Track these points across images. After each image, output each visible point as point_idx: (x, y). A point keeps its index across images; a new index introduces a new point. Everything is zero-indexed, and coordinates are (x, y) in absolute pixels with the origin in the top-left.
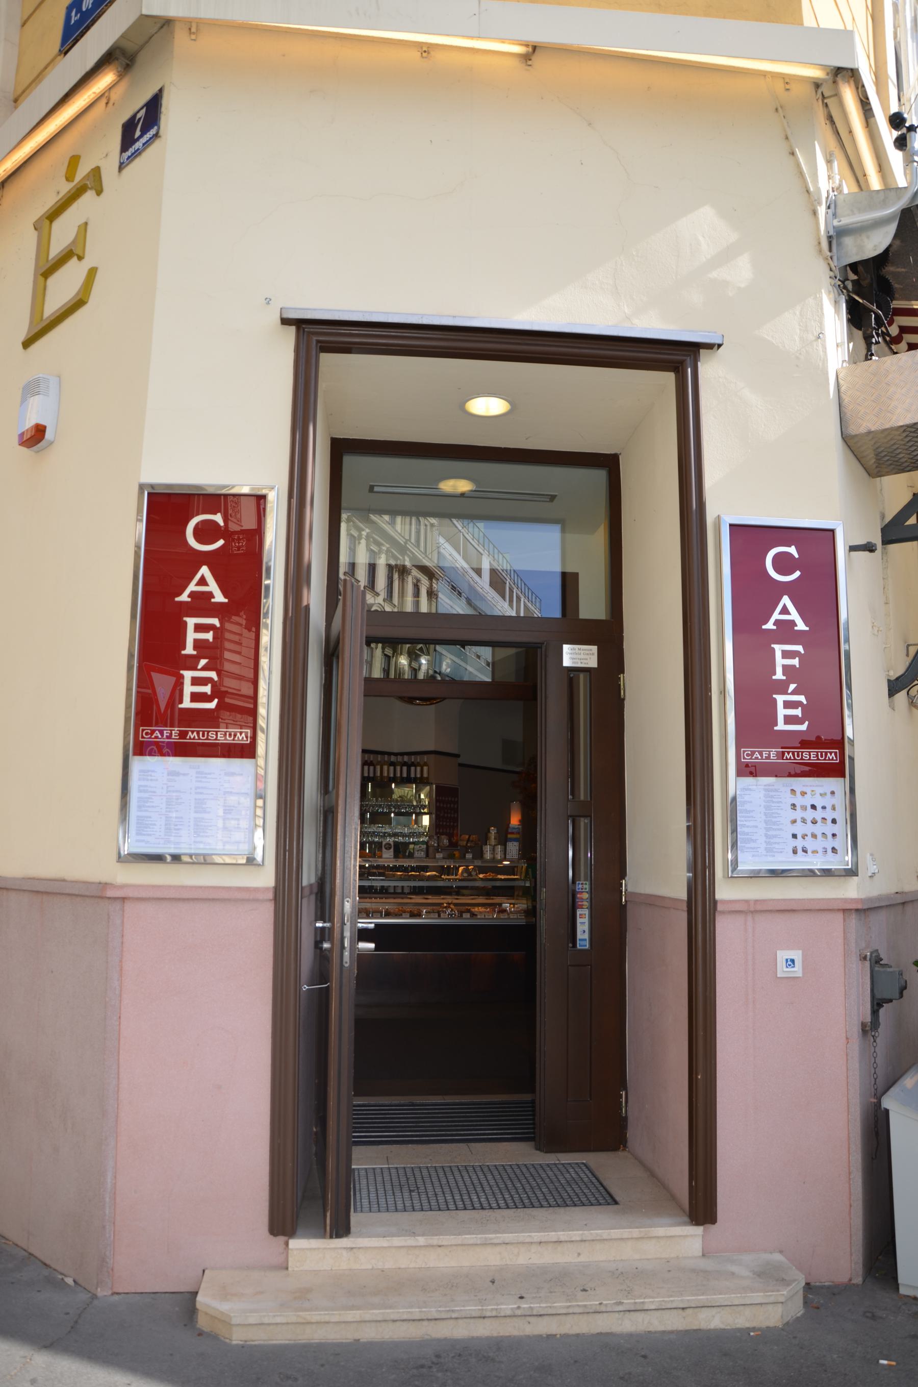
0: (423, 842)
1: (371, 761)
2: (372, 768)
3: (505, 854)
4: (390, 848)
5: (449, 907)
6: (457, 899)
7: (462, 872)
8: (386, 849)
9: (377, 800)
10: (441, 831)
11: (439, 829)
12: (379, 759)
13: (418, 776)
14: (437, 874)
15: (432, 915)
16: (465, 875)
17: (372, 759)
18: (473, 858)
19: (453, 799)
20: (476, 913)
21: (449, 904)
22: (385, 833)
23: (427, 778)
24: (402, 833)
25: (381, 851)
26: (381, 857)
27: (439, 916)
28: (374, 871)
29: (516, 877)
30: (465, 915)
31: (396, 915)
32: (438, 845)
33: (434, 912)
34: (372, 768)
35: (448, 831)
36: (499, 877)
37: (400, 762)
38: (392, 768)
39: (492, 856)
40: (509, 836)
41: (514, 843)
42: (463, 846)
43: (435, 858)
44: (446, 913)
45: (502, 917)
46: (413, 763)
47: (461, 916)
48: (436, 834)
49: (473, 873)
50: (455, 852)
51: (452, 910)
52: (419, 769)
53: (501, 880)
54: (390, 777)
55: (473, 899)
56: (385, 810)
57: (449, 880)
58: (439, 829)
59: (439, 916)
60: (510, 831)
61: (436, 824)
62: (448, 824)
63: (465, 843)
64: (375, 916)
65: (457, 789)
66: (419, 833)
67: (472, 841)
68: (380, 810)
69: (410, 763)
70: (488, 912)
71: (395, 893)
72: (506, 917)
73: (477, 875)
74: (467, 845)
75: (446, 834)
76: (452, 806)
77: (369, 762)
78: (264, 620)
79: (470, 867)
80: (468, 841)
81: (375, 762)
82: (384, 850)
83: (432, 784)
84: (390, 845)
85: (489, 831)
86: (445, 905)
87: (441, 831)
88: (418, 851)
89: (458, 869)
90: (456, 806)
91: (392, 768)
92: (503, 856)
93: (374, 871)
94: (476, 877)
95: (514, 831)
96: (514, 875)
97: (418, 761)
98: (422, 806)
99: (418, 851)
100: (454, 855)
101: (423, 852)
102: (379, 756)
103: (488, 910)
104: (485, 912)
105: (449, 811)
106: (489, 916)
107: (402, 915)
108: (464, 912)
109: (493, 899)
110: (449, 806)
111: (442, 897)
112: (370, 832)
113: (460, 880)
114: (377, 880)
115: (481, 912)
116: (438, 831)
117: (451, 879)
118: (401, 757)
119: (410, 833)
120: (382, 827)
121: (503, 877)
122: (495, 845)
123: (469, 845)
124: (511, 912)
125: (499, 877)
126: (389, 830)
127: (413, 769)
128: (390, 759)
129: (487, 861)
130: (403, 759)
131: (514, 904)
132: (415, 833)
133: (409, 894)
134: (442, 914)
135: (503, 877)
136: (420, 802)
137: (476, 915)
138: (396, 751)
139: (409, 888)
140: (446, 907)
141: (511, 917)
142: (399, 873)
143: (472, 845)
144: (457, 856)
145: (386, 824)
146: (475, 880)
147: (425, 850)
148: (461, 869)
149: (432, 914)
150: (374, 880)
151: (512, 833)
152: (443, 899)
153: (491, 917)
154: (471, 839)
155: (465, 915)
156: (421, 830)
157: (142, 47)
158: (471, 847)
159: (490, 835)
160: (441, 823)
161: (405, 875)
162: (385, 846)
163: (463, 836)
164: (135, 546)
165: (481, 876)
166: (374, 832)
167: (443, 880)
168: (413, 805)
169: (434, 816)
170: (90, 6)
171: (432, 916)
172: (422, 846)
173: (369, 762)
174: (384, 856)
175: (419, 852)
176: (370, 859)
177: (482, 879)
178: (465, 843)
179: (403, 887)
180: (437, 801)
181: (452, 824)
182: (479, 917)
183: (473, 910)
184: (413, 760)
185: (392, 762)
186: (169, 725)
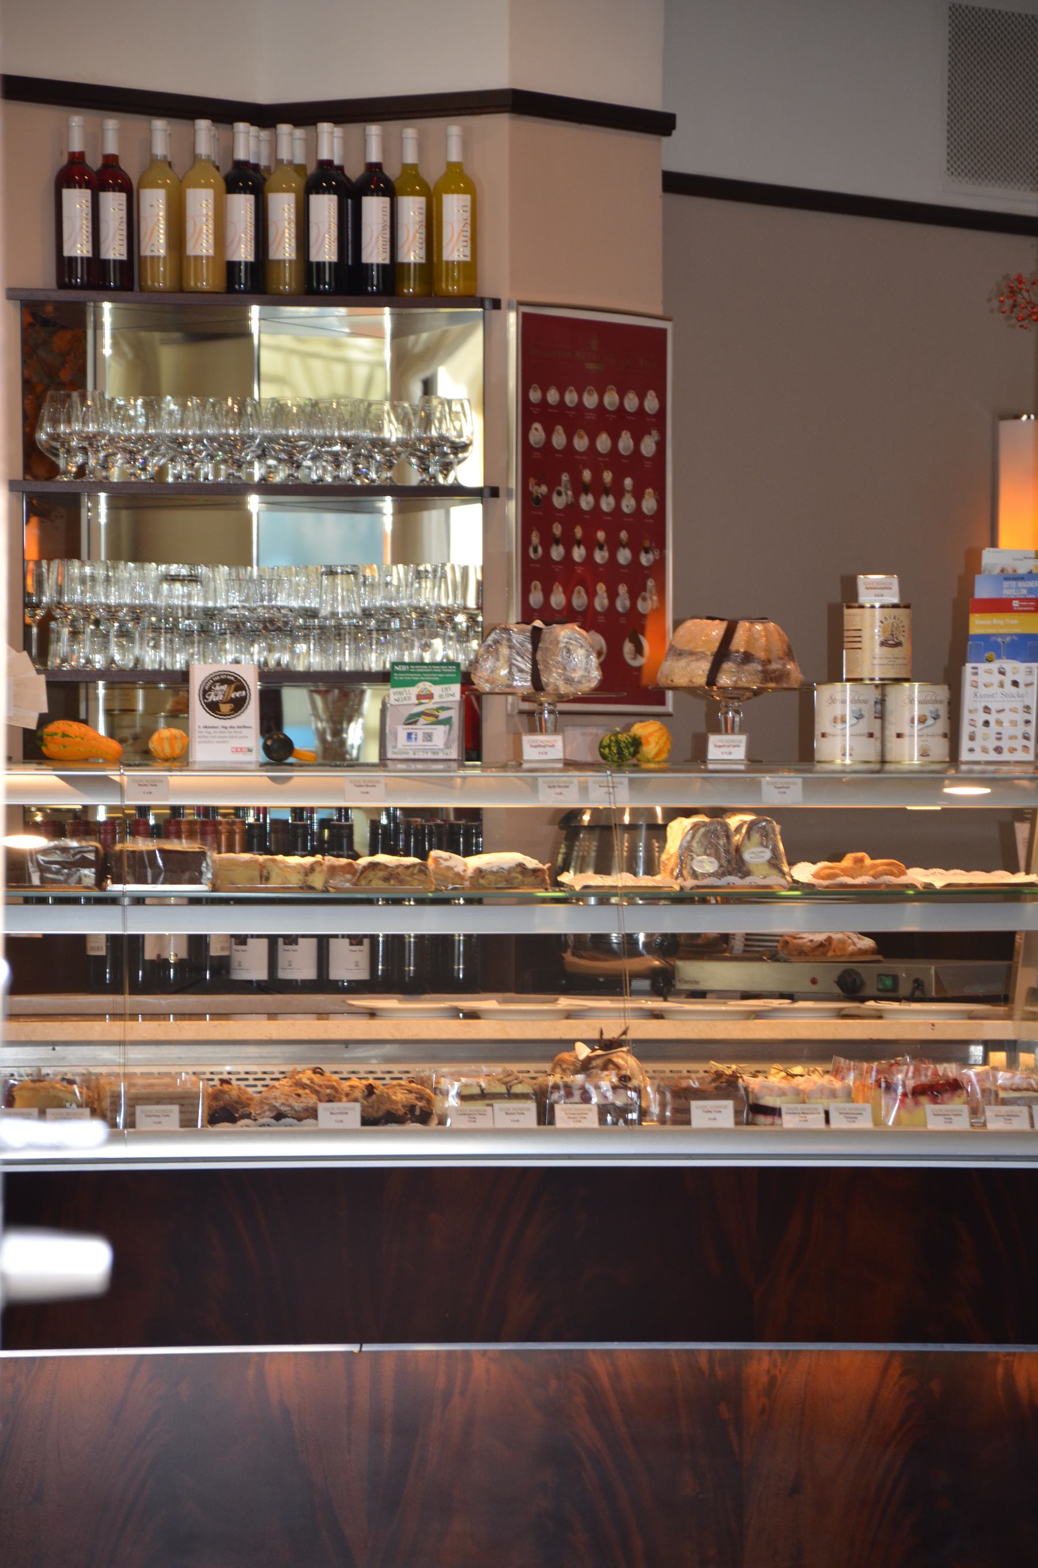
0: (443, 671)
1: (111, 162)
2: (113, 203)
3: (953, 736)
4: (239, 705)
5: (608, 1065)
6: (657, 1015)
7: (686, 852)
8: (213, 708)
9: (152, 409)
10: (557, 599)
11: (547, 593)
12: (160, 148)
13: (412, 254)
14: (531, 863)
15: (501, 1114)
16: (706, 865)
17: (111, 148)
18: (756, 761)
19: (631, 403)
20: (768, 1101)
21: (610, 1045)
22: (210, 614)
23: (470, 269)
24: (312, 613)
25: (186, 729)
26: (180, 760)
27: (545, 1116)
28: (142, 844)
29: (1021, 878)
30: (700, 1112)
31: (279, 1116)
32: (538, 684)
33: (511, 1096)
34: (113, 203)
35: (601, 602)
36: (918, 876)
37: (300, 169)
38: (242, 205)
39: (870, 750)
40: (980, 624)
41: (1009, 665)
42: (691, 690)
43: (516, 761)
44: (586, 1099)
45: (935, 1124)
46: (374, 169)
47: (682, 1117)
48: (528, 615)
49: (756, 855)
50: (639, 729)
51: (624, 1081)
52: (412, 208)
53: (928, 894)
54: (232, 267)
55: (757, 1015)
56: (207, 471)
57: (604, 897)
58: (547, 593)
59: (545, 1116)
60: (983, 591)
61: (883, 1059)
62: (600, 557)
63: (703, 667)
64: (144, 1123)
65: (663, 332)
66: (422, 613)
67: (747, 658)
68: (177, 471)
69: (355, 172)
70: (849, 1096)
71: (274, 985)
72: (962, 1123)
73: (774, 863)
74: (712, 678)
75: (587, 620)
76: (626, 442)
77: (94, 163)
78: (626, 781)
79: (733, 821)
80: (722, 654)
81: (131, 167)
82: (199, 714)
83: (496, 304)
84: (240, 685)
85: (850, 596)
86: (583, 1051)
87: (557, 599)
88: (412, 720)
89: (658, 831)
90: (648, 446)
91: (242, 205)
92: (940, 749)
93: (142, 844)
94: (774, 880)
95: (1009, 590)
96: (1014, 870)
97: (410, 157)
98: (435, 445)
99: (412, 720)
100: (637, 743)
101: (440, 733)
102: (159, 125)
103: (851, 1079)
104: (833, 1094)
105: (608, 477)
106: (851, 1117)
107: (312, 1113)
108: (700, 1094)
109: (879, 1015)
110: (603, 443)
111: (565, 1002)
112: (112, 612)
113: (681, 899)
114: (161, 900)
115: (801, 1097)
116: (536, 598)
117: (613, 891)
118: (299, 133)
119: (367, 613)
120: (193, 579)
121: (939, 878)
122: (884, 685)
123: (725, 680)
124: (992, 1096)
125: (918, 876)
126: (235, 600)
127: (374, 208)
128: (231, 149)
129: (837, 781)
130: (312, 145)
131: (1011, 1047)
132: (393, 613)
133: (357, 988)
134: (561, 1111)
135: (939, 878)
136: (427, 422)
137: (774, 1112)
138: (264, 95)
139: (362, 954)
140: (585, 1066)
141: (991, 1126)
142: (294, 860)
143: (744, 681)
144: (650, 749)
145: (212, 563)
146: (764, 897)
147: (455, 714)
148: (678, 830)
149: (499, 1105)
150: (139, 900)
151: (999, 606)
152: (569, 1015)
153: (865, 1123)
154: (739, 643)
155: (700, 1112)
156: (430, 596)
157: (860, 735)
158: (736, 694)
159: (852, 617)
160: (557, 553)
161: (333, 870)
162: (205, 693)
163: (690, 625)
164: (748, 1019)
165: (804, 872)
166: (137, 613)
167: (572, 898)
168: (384, 443)
169: (512, 508)
170: (786, 638)
171: (503, 1122)
172: (436, 690)
173: (94, 163)
174: (201, 752)
175: (420, 728)
176: (114, 775)
177: (809, 892)
178: (698, 671)
179: (323, 942)
180: (529, 413)
181: (624, 556)
182: (789, 1121)
183: (755, 1083)
184: (374, 157)
185: (242, 167)
186: (237, 848)
